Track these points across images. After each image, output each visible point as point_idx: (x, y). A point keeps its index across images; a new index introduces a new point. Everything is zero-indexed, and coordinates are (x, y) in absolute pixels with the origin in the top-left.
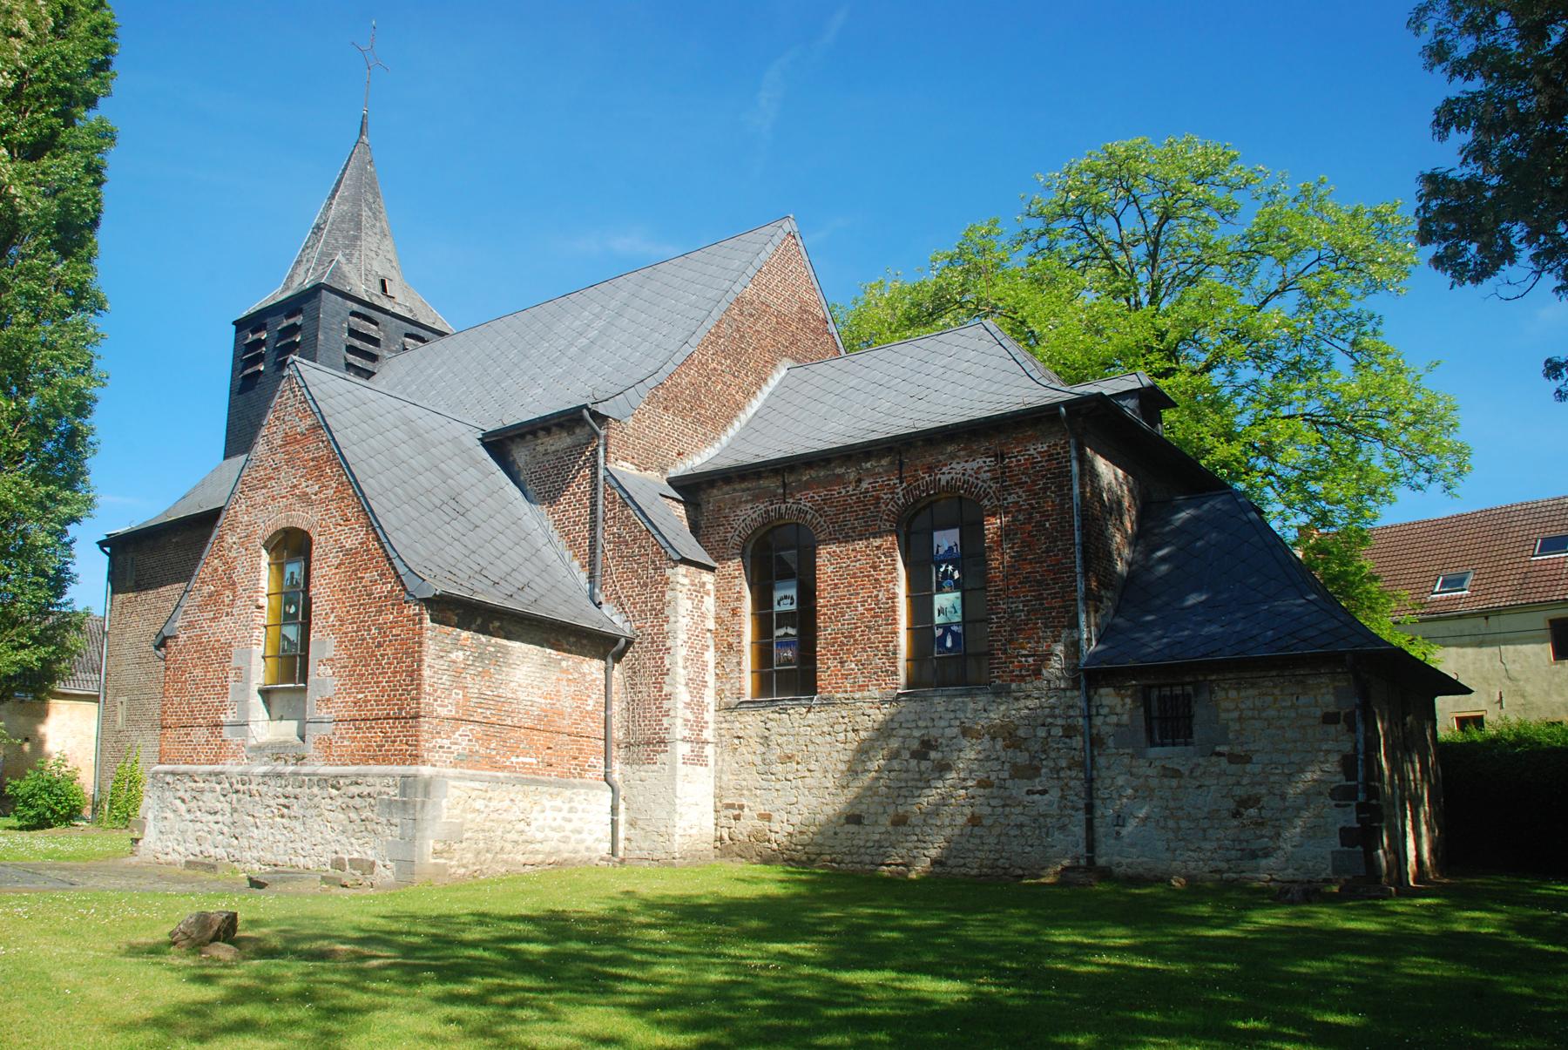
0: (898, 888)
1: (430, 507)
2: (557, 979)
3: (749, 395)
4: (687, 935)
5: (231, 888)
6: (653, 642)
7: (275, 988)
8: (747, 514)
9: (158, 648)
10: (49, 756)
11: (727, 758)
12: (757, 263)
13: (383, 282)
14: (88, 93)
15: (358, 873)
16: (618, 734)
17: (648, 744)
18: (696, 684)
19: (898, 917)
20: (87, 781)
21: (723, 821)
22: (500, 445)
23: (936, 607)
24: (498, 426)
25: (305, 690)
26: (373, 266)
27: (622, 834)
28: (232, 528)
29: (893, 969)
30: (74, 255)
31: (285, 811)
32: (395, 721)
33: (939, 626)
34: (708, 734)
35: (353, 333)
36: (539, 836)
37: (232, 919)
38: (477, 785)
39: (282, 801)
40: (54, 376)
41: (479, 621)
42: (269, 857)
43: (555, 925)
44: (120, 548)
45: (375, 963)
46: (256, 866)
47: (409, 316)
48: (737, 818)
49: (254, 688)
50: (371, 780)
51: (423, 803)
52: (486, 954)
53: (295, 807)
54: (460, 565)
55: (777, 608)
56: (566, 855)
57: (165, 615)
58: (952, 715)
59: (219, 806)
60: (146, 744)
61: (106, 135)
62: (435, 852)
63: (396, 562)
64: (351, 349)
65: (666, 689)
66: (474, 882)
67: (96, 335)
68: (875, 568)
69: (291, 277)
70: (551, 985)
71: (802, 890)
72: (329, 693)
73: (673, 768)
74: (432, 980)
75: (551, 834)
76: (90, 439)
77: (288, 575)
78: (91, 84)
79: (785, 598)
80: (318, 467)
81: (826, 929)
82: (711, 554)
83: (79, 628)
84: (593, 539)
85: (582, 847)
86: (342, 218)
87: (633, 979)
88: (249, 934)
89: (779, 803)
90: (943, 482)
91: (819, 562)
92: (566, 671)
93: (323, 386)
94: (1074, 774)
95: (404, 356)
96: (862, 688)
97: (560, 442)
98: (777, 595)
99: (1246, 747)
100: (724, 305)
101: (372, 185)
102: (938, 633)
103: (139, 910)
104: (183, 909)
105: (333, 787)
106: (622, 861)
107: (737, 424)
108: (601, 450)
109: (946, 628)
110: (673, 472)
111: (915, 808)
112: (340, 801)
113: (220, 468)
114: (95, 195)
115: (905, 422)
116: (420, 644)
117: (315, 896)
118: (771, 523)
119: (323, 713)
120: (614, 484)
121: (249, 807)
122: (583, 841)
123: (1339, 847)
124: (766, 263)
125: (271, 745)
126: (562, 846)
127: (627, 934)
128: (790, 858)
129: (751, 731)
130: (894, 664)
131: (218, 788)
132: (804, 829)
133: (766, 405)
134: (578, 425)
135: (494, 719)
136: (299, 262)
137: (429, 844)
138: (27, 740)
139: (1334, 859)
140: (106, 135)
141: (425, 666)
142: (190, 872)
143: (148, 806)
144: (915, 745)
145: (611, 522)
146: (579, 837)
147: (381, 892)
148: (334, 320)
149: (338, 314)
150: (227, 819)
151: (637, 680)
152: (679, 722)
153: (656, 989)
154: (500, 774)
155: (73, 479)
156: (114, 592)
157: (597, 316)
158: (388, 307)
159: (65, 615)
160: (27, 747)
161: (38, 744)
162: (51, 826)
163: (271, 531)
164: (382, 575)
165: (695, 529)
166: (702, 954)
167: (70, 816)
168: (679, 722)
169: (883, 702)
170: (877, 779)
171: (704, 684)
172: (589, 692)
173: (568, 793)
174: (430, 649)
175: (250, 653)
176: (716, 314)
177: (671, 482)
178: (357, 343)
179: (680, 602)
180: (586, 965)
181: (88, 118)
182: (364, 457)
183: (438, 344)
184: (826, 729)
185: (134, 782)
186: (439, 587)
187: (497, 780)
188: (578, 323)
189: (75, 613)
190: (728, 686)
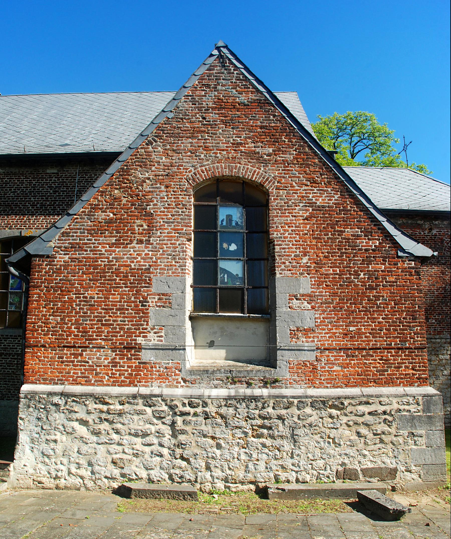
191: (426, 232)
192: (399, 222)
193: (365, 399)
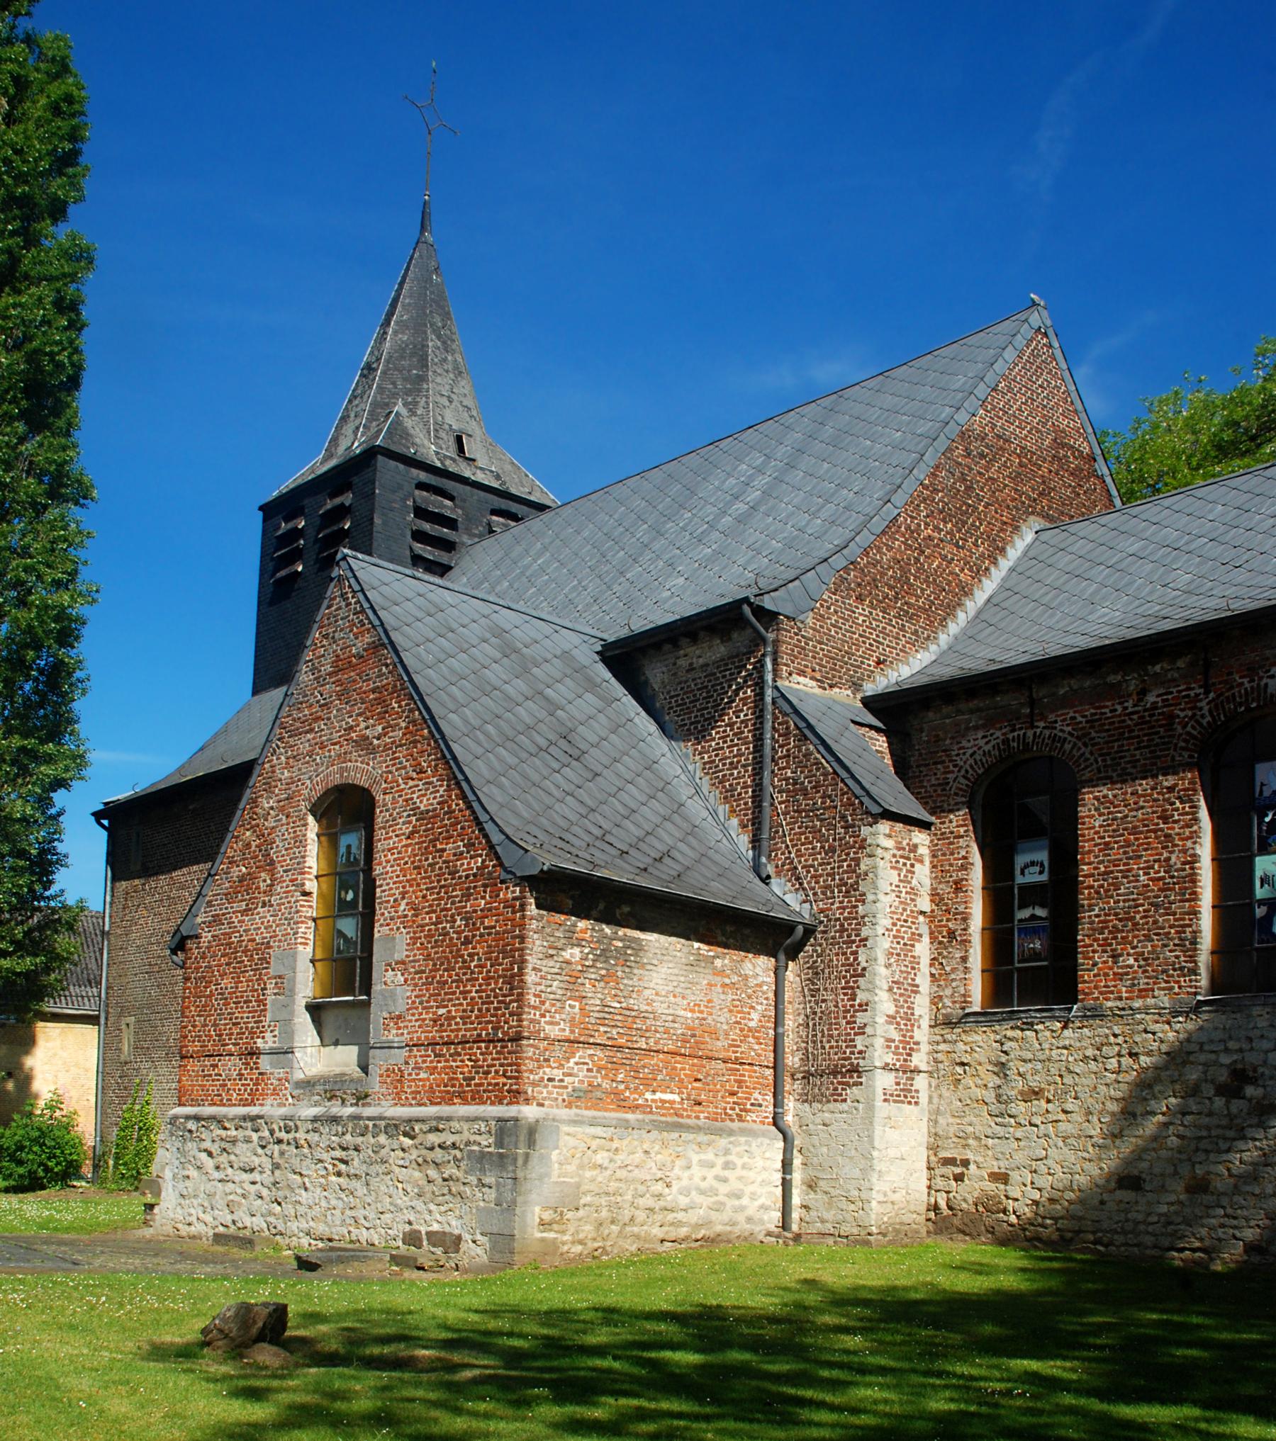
0: (1192, 1285)
1: (533, 750)
2: (716, 1401)
3: (979, 573)
4: (894, 1344)
5: (273, 1271)
6: (842, 930)
7: (340, 1406)
8: (977, 746)
9: (174, 952)
10: (36, 1097)
11: (946, 1094)
12: (990, 378)
13: (459, 440)
14: (55, 199)
15: (439, 1251)
16: (792, 1060)
17: (835, 1073)
18: (904, 989)
19: (1198, 1326)
20: (86, 1127)
21: (940, 1183)
22: (627, 659)
23: (1258, 874)
24: (624, 633)
25: (367, 1004)
26: (448, 418)
27: (796, 1200)
28: (269, 789)
29: (1195, 1403)
30: (48, 427)
31: (342, 1167)
32: (488, 1043)
33: (1261, 902)
34: (920, 1060)
35: (421, 513)
36: (683, 1201)
37: (280, 1313)
38: (599, 1131)
39: (338, 1153)
40: (29, 592)
41: (601, 906)
42: (321, 1229)
43: (707, 1325)
44: (116, 817)
45: (468, 1374)
46: (305, 1241)
47: (495, 484)
48: (959, 1178)
49: (301, 1003)
50: (456, 1125)
51: (527, 1156)
52: (616, 1365)
53: (356, 1163)
54: (575, 829)
55: (1020, 880)
56: (719, 1228)
57: (183, 908)
59: (257, 1161)
60: (160, 1080)
61: (81, 257)
62: (542, 1223)
63: (489, 827)
64: (419, 536)
65: (861, 997)
66: (594, 1264)
67: (80, 532)
68: (1165, 819)
69: (335, 440)
70: (708, 1410)
71: (1054, 1283)
72: (400, 1007)
73: (871, 1107)
74: (547, 1398)
75: (699, 1199)
76: (79, 674)
77: (343, 850)
78: (57, 186)
79: (1032, 865)
80: (380, 701)
81: (1091, 1340)
82: (925, 804)
83: (71, 927)
84: (758, 788)
85: (741, 1218)
86: (401, 351)
87: (821, 1405)
88: (301, 1333)
89: (1020, 1158)
91: (1083, 812)
92: (721, 973)
93: (383, 589)
95: (489, 542)
96: (1143, 993)
97: (713, 651)
98: (1020, 860)
100: (942, 443)
101: (440, 303)
102: (1260, 912)
103: (161, 1300)
104: (221, 1298)
105: (406, 1134)
106: (797, 1238)
107: (962, 617)
108: (768, 661)
110: (870, 689)
111: (1222, 1169)
112: (414, 1154)
113: (248, 704)
114: (71, 342)
115: (1212, 603)
116: (522, 939)
117: (383, 1282)
118: (1007, 760)
119: (392, 1035)
120: (788, 709)
121: (295, 1162)
122: (742, 1208)
124: (1005, 377)
125: (323, 1080)
126: (714, 1216)
127: (809, 1340)
128: (1040, 1236)
129: (981, 1055)
130: (1193, 959)
131: (255, 1136)
132: (1056, 1194)
133: (1004, 587)
134: (737, 628)
135: (622, 1041)
136: (344, 419)
137: (534, 1211)
138: (10, 1075)
140: (81, 257)
141: (528, 970)
142: (220, 1249)
143: (165, 1161)
144: (1223, 1076)
145: (783, 763)
146: (737, 1203)
147: (470, 1276)
148: (394, 491)
149: (400, 487)
150: (267, 1178)
151: (820, 984)
152: (879, 1042)
153: (854, 1420)
154: (630, 1116)
155: (57, 725)
156: (114, 879)
157: (760, 471)
158: (467, 473)
159: (54, 911)
160: (10, 1086)
161: (25, 1081)
162: (43, 1188)
163: (320, 790)
164: (469, 846)
165: (902, 768)
166: (914, 1371)
167: (67, 1174)
168: (879, 1042)
169: (1175, 1013)
170: (1166, 1125)
171: (915, 989)
172: (753, 1002)
173: (723, 1142)
174: (536, 945)
175: (294, 957)
176: (930, 458)
177: (868, 703)
178: (427, 527)
179: (881, 873)
180: (754, 1383)
181: (58, 234)
182: (442, 684)
183: (537, 523)
184: (1090, 1052)
185: (146, 1130)
186: (548, 861)
187: (626, 1125)
188: (732, 481)
189: (65, 908)
190: (948, 992)
191: (1129, 704)
192: (1062, 692)
193: (434, 1123)
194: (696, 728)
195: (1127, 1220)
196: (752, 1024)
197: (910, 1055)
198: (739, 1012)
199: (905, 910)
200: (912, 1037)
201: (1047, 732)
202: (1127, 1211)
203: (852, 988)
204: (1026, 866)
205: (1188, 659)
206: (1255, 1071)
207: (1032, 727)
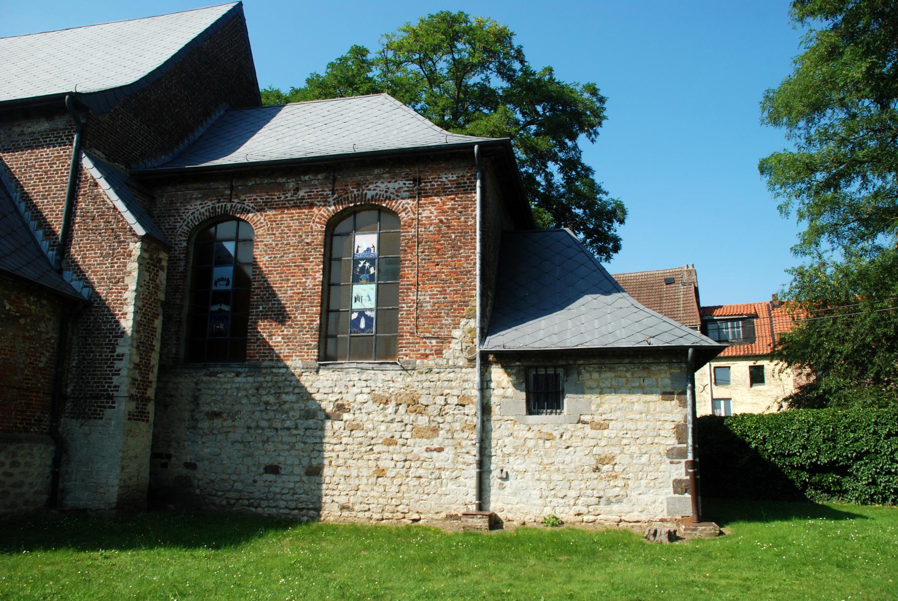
23: (354, 295)
58: (364, 384)
90: (369, 196)
94: (465, 435)
99: (604, 417)
102: (355, 316)
109: (362, 313)
123: (672, 495)
139: (668, 504)
146: (18, 491)
173: (12, 448)
192: (250, 184)
194: (20, 171)
195: (270, 492)
196: (41, 365)
197: (146, 390)
198: (32, 356)
199: (151, 298)
200: (148, 378)
201: (239, 205)
202: (269, 487)
203: (113, 344)
204: (219, 280)
205: (324, 175)
206: (349, 405)
207: (231, 202)
